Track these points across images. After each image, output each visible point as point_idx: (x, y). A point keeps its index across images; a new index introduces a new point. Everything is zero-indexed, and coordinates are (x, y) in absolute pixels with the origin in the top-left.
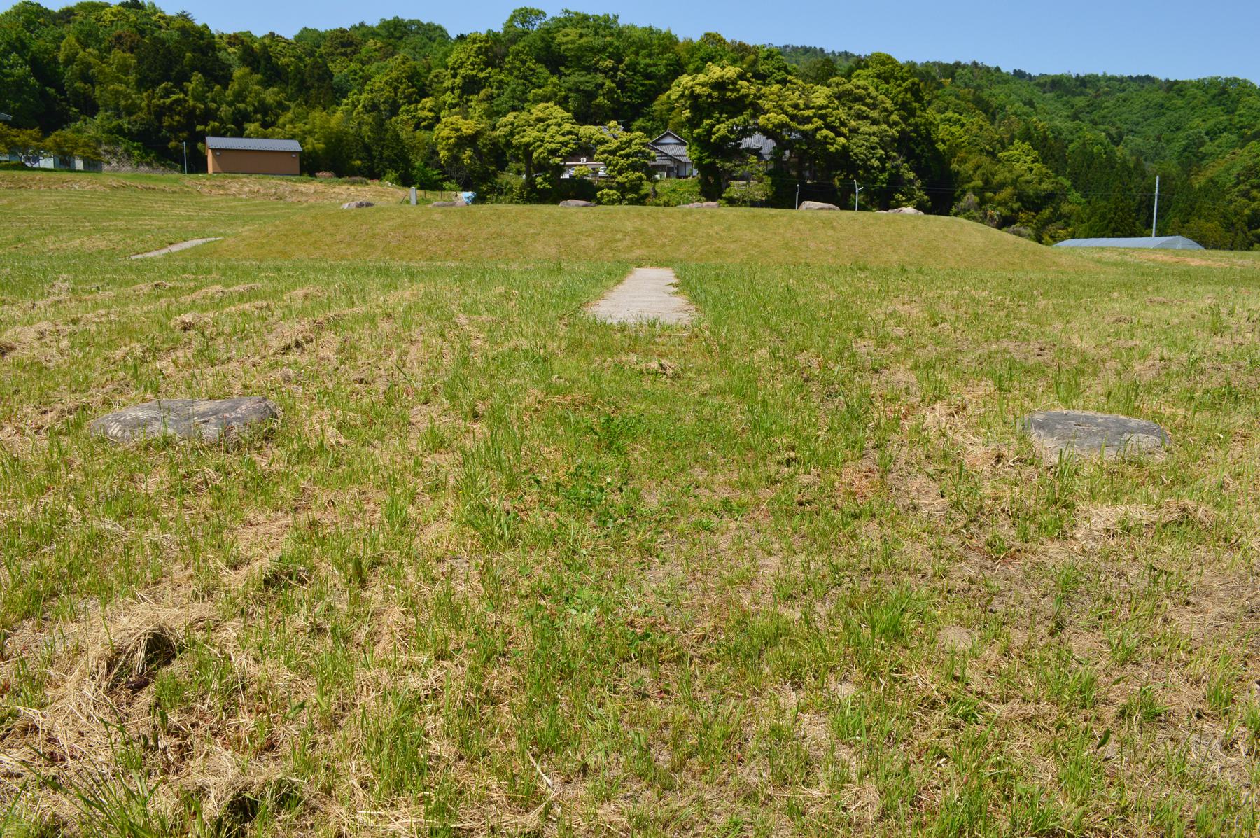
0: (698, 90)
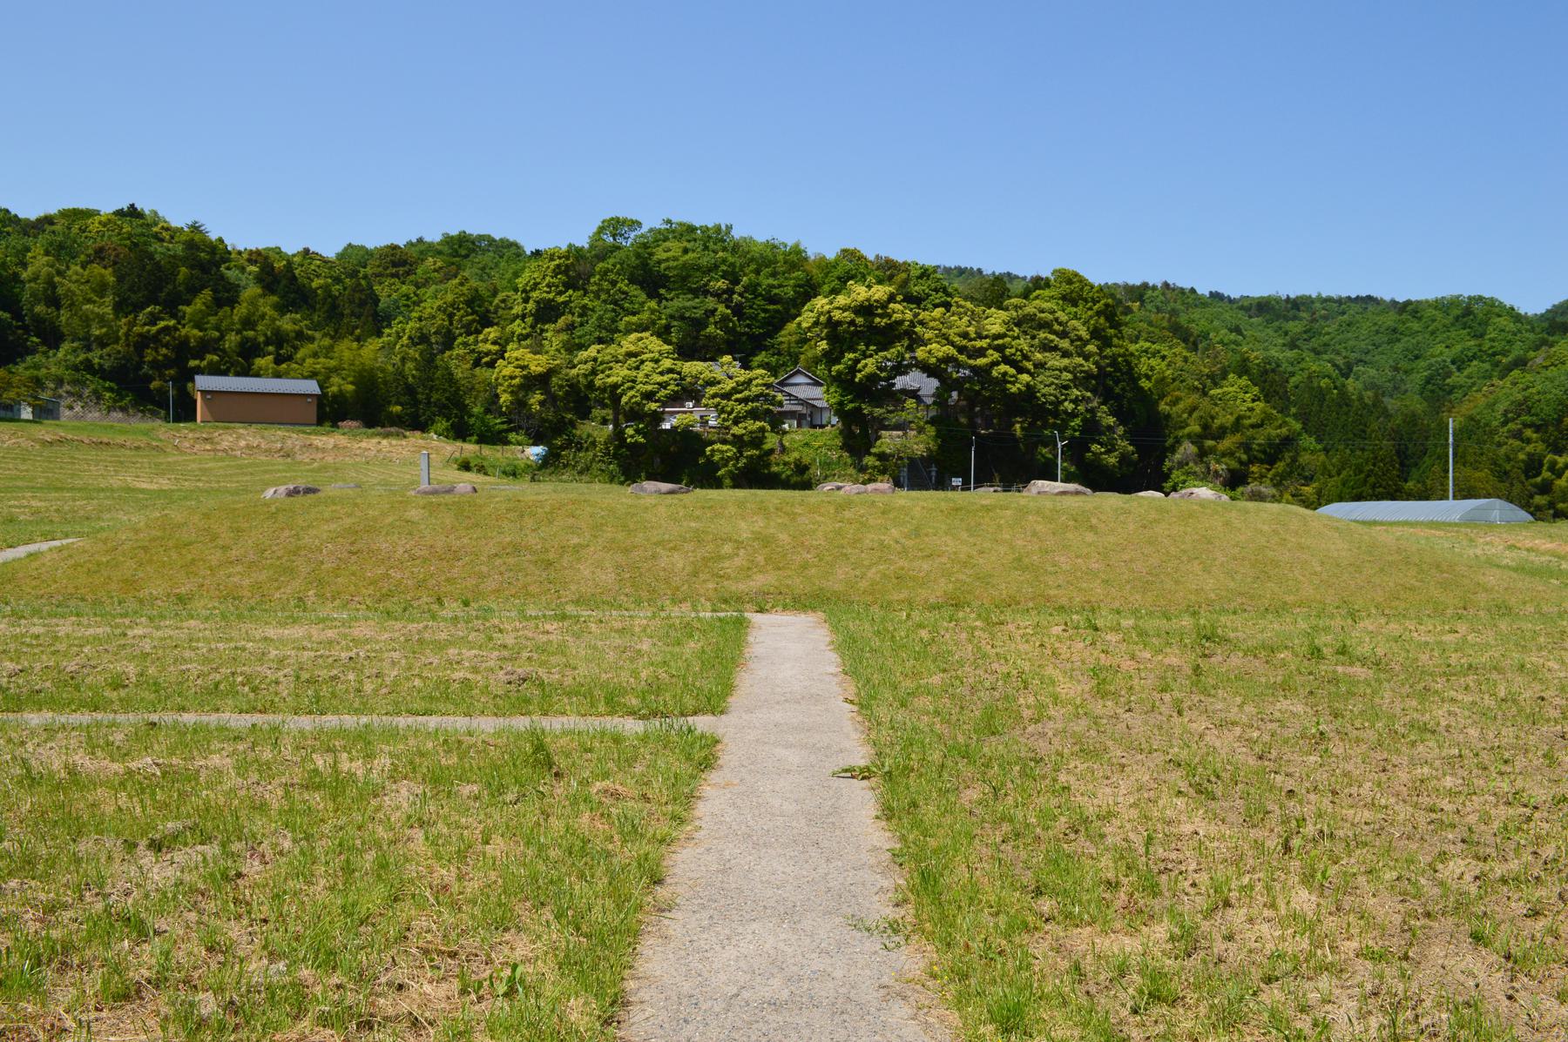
0: (837, 315)
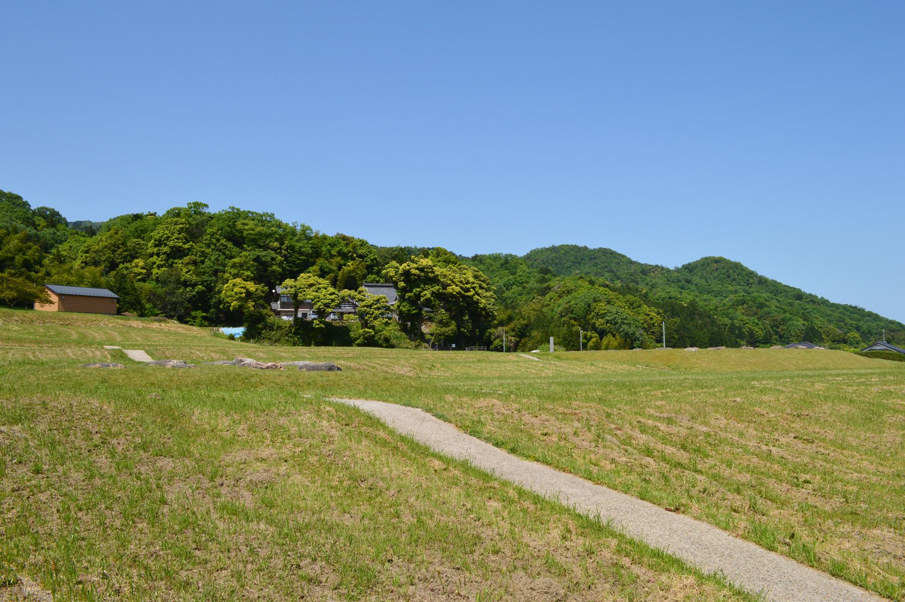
0: (413, 271)
